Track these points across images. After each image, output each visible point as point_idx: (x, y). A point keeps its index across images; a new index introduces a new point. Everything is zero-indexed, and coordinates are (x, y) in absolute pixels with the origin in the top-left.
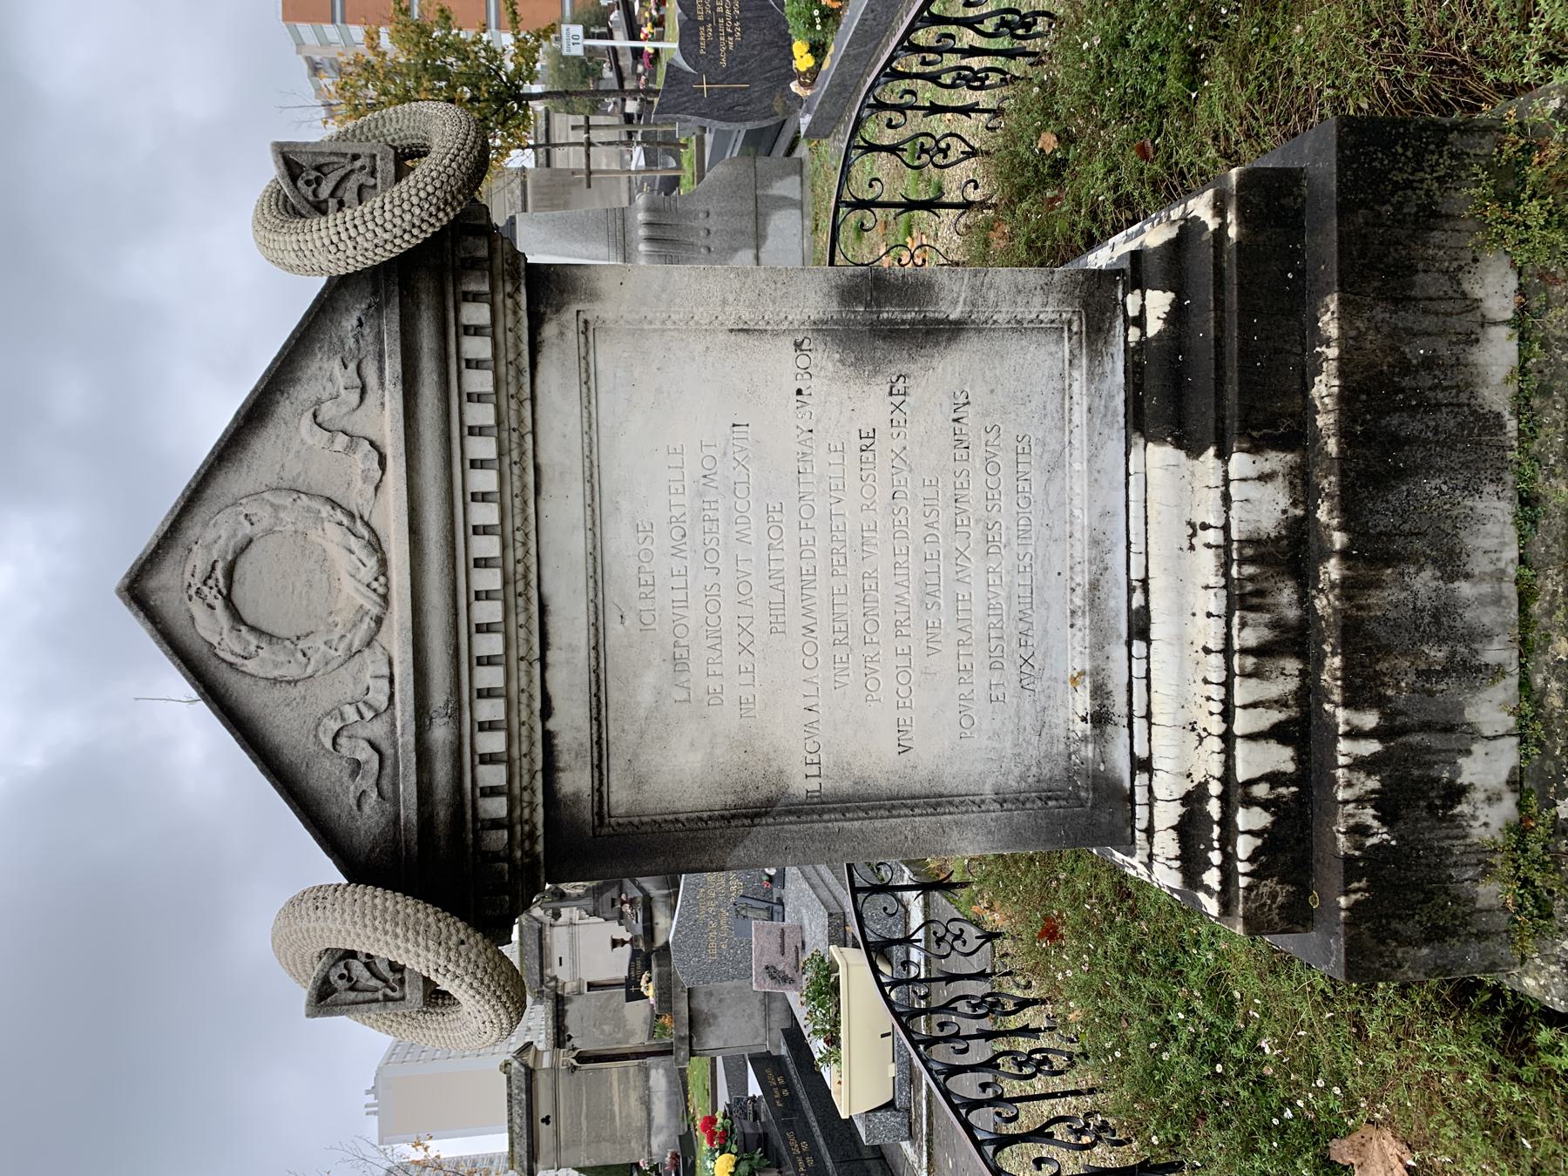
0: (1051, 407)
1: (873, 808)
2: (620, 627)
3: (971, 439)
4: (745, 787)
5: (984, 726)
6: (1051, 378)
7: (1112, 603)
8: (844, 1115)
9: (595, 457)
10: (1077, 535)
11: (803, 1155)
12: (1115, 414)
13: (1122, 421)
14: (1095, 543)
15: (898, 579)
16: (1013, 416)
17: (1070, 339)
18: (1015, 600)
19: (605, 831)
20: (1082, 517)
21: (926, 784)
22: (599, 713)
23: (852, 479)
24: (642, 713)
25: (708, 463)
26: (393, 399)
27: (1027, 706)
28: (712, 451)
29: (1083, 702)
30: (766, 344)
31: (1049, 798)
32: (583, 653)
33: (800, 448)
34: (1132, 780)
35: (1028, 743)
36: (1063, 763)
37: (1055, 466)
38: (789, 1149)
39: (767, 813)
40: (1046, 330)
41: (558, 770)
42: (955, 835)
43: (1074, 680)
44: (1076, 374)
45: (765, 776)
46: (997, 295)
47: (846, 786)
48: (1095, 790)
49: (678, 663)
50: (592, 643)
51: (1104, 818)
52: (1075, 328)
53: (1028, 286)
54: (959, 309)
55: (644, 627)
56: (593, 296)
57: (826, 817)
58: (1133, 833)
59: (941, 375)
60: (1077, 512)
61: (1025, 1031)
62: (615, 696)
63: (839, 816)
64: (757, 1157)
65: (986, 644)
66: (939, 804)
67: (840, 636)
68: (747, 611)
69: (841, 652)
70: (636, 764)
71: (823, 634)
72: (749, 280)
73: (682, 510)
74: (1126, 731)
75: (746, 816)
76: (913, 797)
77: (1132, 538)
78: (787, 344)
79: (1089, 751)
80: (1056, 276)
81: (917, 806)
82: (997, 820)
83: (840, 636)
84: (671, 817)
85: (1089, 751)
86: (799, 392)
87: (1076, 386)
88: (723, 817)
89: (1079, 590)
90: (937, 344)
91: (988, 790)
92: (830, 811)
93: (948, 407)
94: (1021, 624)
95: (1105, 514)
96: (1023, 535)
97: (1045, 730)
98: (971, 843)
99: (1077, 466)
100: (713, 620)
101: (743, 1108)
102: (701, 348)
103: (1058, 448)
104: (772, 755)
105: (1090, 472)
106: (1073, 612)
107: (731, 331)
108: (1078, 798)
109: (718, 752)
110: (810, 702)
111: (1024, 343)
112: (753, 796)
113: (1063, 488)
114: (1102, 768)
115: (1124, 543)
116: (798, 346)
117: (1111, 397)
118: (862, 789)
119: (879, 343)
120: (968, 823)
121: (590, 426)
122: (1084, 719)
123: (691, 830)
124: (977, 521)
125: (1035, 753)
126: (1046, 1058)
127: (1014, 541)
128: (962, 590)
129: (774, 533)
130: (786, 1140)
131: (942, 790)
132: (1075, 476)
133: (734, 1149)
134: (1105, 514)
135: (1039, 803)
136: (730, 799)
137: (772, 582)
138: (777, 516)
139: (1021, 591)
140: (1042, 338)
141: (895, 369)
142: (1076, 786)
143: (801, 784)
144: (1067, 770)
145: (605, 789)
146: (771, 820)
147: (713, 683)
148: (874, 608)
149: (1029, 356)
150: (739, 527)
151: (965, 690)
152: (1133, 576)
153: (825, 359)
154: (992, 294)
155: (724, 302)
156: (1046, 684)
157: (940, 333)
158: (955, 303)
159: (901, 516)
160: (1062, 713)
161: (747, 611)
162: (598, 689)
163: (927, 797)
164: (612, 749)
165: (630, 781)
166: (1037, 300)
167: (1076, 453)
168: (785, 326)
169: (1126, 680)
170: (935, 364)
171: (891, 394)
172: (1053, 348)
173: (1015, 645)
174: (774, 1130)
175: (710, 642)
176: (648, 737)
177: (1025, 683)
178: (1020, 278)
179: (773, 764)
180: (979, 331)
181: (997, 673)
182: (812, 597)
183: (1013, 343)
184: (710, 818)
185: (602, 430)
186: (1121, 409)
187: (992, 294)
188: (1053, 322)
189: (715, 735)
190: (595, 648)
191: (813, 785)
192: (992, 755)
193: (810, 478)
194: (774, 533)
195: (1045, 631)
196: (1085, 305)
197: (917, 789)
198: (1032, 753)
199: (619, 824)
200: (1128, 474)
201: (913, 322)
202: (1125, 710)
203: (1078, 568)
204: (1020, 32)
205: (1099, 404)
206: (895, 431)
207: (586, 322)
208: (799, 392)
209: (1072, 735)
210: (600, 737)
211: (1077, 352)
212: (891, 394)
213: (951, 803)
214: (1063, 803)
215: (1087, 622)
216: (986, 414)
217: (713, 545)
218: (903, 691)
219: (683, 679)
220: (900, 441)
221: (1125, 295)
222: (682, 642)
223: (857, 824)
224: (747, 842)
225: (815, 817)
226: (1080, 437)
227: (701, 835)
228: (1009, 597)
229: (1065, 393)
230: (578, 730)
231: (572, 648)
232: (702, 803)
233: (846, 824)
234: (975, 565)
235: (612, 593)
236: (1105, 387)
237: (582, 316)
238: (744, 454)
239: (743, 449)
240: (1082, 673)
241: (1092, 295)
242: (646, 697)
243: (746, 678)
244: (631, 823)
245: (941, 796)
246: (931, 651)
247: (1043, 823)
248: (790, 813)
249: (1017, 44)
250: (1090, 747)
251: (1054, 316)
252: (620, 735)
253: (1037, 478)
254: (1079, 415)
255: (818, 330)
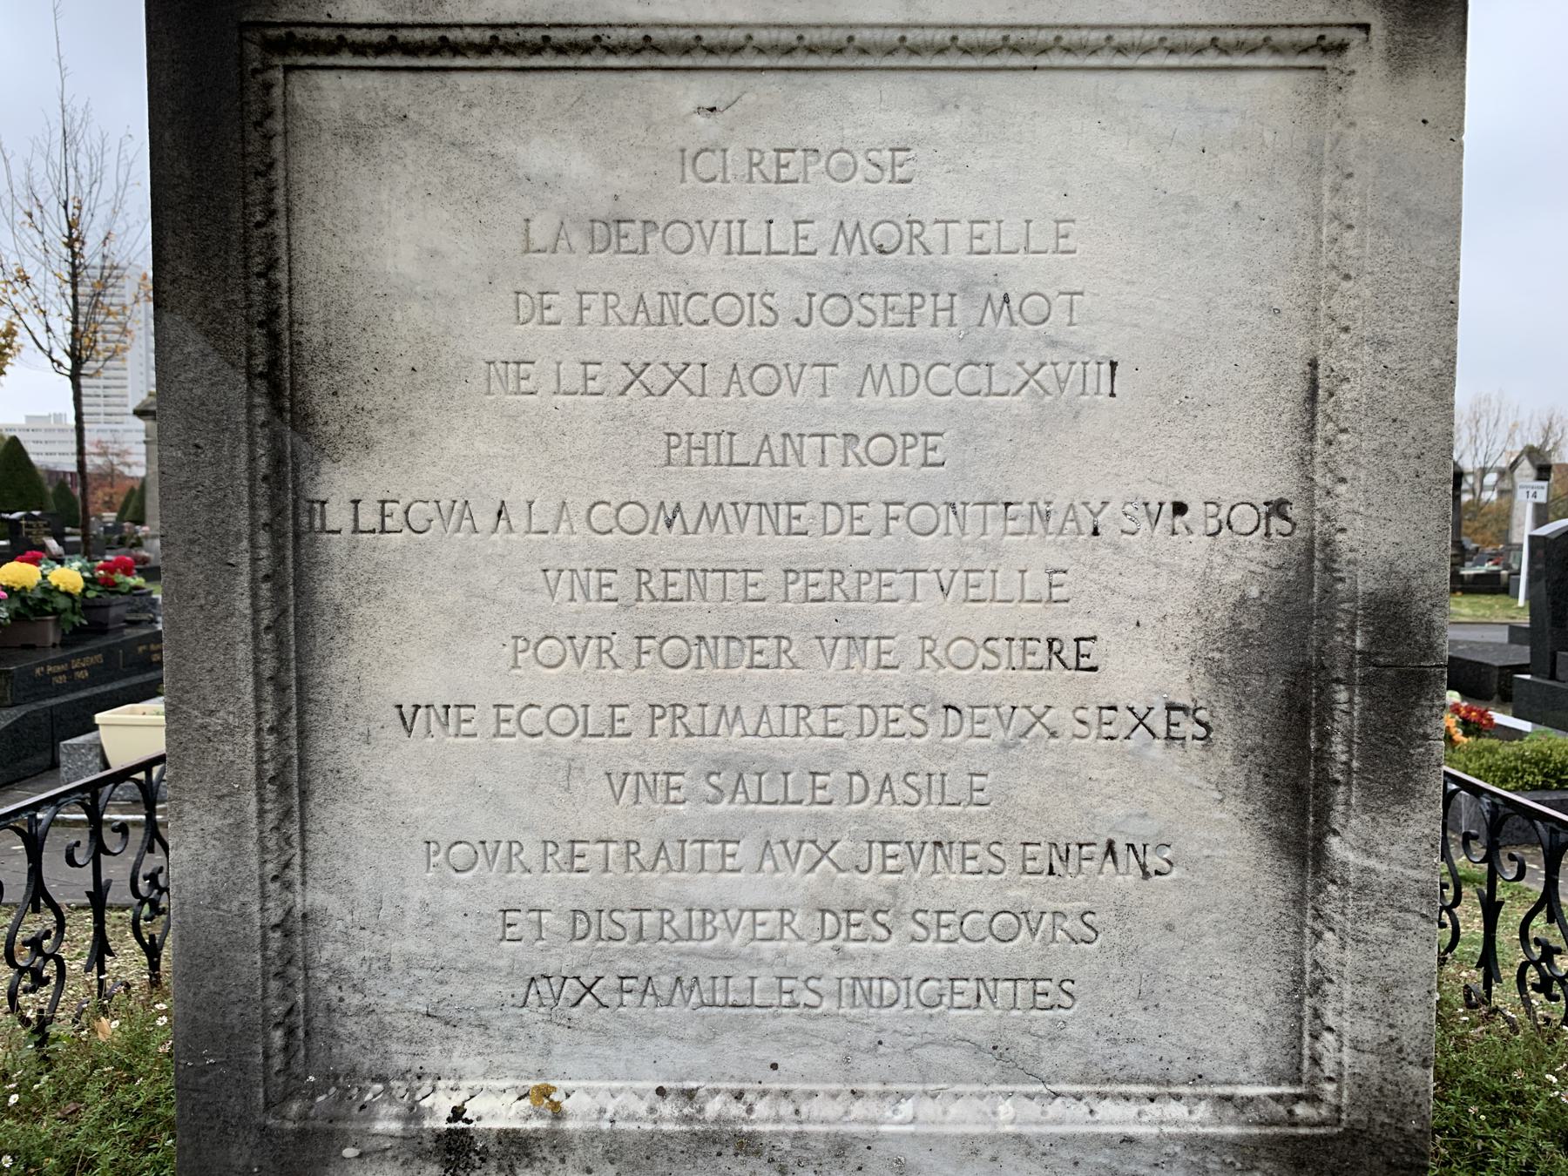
0: (1131, 1053)
1: (280, 643)
2: (689, 105)
3: (1070, 880)
4: (337, 367)
6: (1195, 1055)
8: (100, 718)
9: (1056, 59)
10: (858, 1109)
11: (70, 672)
15: (774, 714)
16: (1115, 971)
17: (1278, 1098)
19: (254, 52)
21: (330, 763)
23: (989, 619)
24: (505, 147)
25: (1033, 306)
27: (491, 989)
28: (1059, 316)
30: (1284, 440)
31: (290, 1033)
33: (1060, 504)
35: (412, 990)
36: (367, 1063)
37: (1005, 1061)
38: (81, 655)
39: (279, 411)
40: (1296, 1045)
42: (213, 822)
43: (545, 1092)
44: (1203, 1110)
45: (359, 410)
47: (332, 588)
48: (302, 1135)
49: (608, 229)
50: (658, 35)
52: (1301, 1110)
54: (1351, 857)
55: (688, 158)
56: (1401, 61)
57: (264, 538)
59: (1208, 821)
60: (907, 1108)
61: (101, 949)
63: (265, 566)
64: (76, 619)
65: (626, 900)
66: (284, 789)
67: (656, 585)
69: (622, 584)
70: (396, 132)
71: (664, 546)
72: (1425, 400)
75: (274, 363)
76: (302, 733)
78: (1281, 484)
79: (387, 1124)
80: (1416, 1072)
81: (282, 740)
82: (244, 916)
83: (656, 585)
84: (279, 200)
85: (387, 1124)
87: (1176, 1110)
88: (274, 314)
89: (737, 1109)
90: (1274, 810)
91: (315, 897)
92: (278, 549)
93: (1138, 831)
94: (667, 980)
96: (860, 990)
97: (438, 1027)
98: (195, 857)
99: (1006, 1109)
100: (699, 308)
101: (144, 609)
102: (1279, 300)
103: (1045, 1070)
104: (404, 428)
105: (993, 1139)
106: (690, 1095)
107: (1314, 365)
108: (288, 1097)
109: (415, 309)
110: (517, 518)
111: (1270, 997)
112: (318, 384)
113: (957, 1079)
114: (349, 1152)
116: (1278, 508)
118: (325, 621)
119: (1279, 684)
120: (239, 851)
122: (457, 1113)
123: (246, 240)
124: (893, 889)
125: (391, 1003)
126: (46, 981)
128: (745, 852)
129: (880, 447)
130: (92, 653)
131: (317, 798)
132: (985, 1106)
133: (91, 594)
135: (278, 1010)
136: (313, 334)
137: (776, 441)
138: (915, 454)
139: (739, 982)
142: (315, 1090)
143: (340, 489)
144: (352, 1072)
145: (346, 59)
146: (261, 415)
147: (564, 304)
148: (713, 658)
149: (1241, 1008)
151: (531, 854)
153: (1246, 564)
154: (1382, 930)
155: (1381, 344)
156: (537, 1031)
157: (1297, 817)
158: (1368, 849)
160: (474, 1063)
162: (560, 50)
163: (303, 764)
164: (432, 80)
165: (361, 116)
166: (1366, 1030)
170: (1231, 804)
171: (1171, 707)
172: (1257, 1061)
173: (625, 965)
174: (110, 640)
175: (652, 300)
176: (453, 158)
177: (543, 985)
178: (1415, 992)
179: (385, 431)
180: (1298, 901)
181: (564, 925)
182: (742, 524)
183: (1268, 975)
184: (273, 287)
187: (1382, 930)
188: (1316, 1061)
191: (338, 516)
192: (387, 911)
193: (994, 528)
194: (880, 447)
195: (654, 1033)
196: (1353, 1135)
197: (322, 744)
198: (390, 996)
199: (268, 87)
201: (1323, 757)
203: (786, 1109)
204: (1532, 975)
206: (1090, 715)
207: (1342, 47)
208: (1180, 508)
209: (427, 1084)
211: (1251, 1114)
212: (1171, 707)
213: (287, 814)
214: (277, 1063)
215: (668, 1127)
216: (1121, 913)
217: (860, 313)
218: (532, 719)
220: (1070, 726)
222: (654, 240)
223: (244, 605)
224: (214, 360)
225: (264, 515)
226: (1069, 1118)
227: (235, 258)
228: (725, 955)
229: (1162, 1086)
232: (306, 272)
233: (244, 581)
234: (799, 881)
237: (1356, 37)
238: (1051, 385)
239: (1061, 383)
240: (558, 1113)
241: (1375, 1149)
242: (539, 155)
243: (572, 379)
244: (269, 114)
245: (304, 795)
246: (616, 780)
247: (233, 1018)
248: (278, 461)
249: (1509, 974)
250: (395, 1127)
251: (1329, 1068)
252: (466, 99)
253: (982, 1022)
254: (1116, 1117)
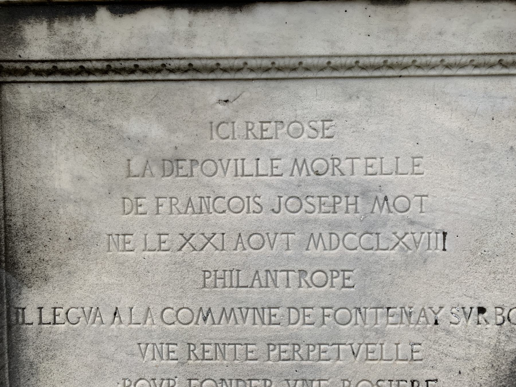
2: (214, 99)
9: (412, 72)
22: (117, 71)
24: (116, 122)
28: (415, 208)
32: (184, 51)
33: (416, 308)
41: (51, 22)
45: (42, 260)
49: (172, 164)
50: (196, 63)
55: (214, 127)
62: (138, 92)
70: (59, 115)
71: (202, 330)
73: (348, 172)
86: (482, 310)
104: (65, 270)
109: (71, 208)
118: (25, 371)
121: (447, 66)
147: (148, 203)
150: (326, 237)
161: (229, 244)
164: (78, 88)
165: (41, 107)
175: (196, 201)
176: (89, 128)
179: (56, 271)
182: (244, 319)
185: (441, 82)
189: (89, 204)
190: (190, 68)
191: (31, 316)
208: (482, 310)
210: (89, 72)
217: (306, 206)
219: (155, 169)
222: (196, 170)
230: (96, 45)
231: (190, 37)
235: (254, 90)
238: (411, 245)
239: (417, 243)
242: (134, 126)
252: (94, 97)
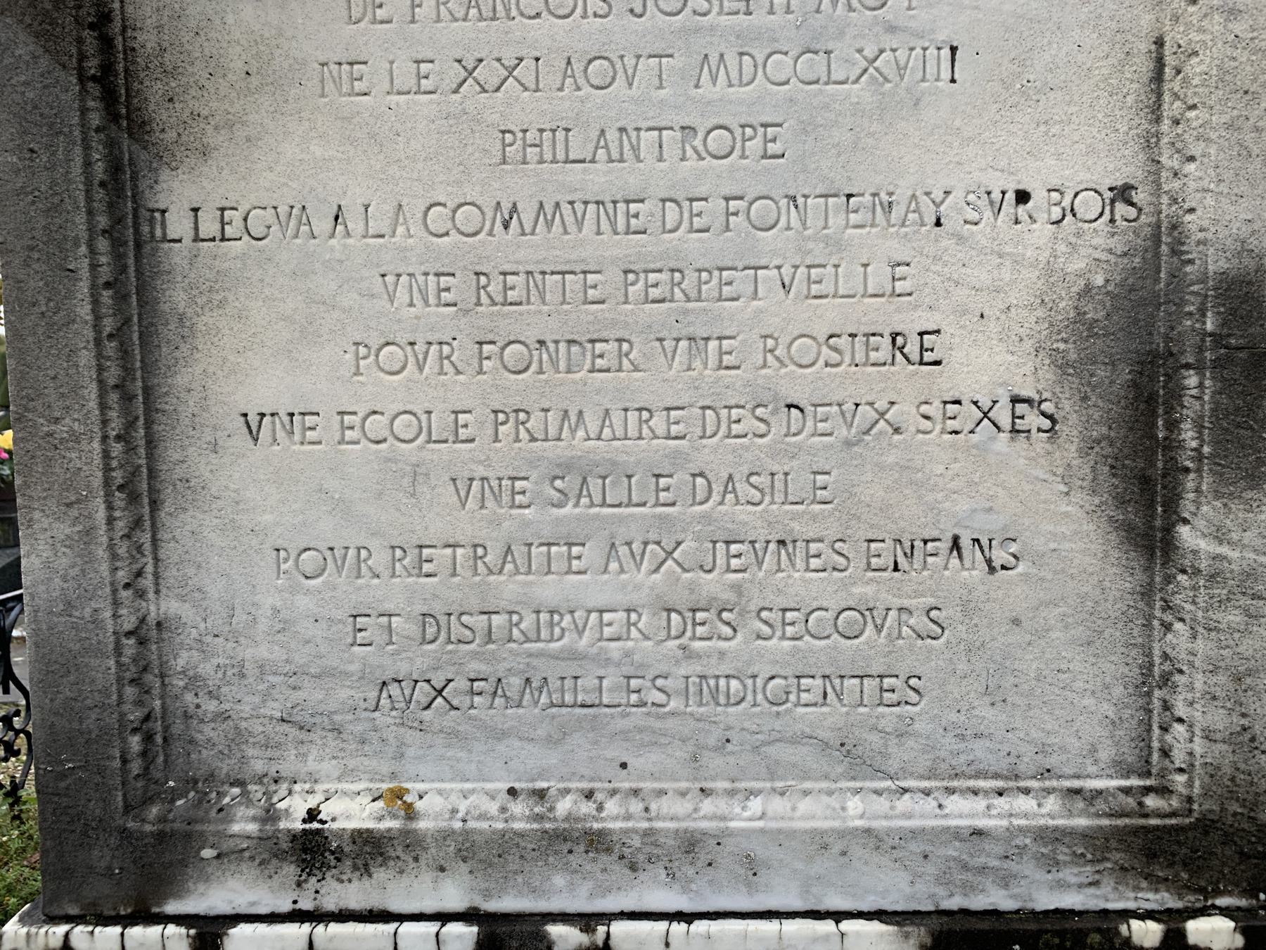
0: (979, 750)
3: (914, 576)
4: (172, 73)
5: (303, 602)
6: (1042, 750)
7: (559, 880)
10: (707, 806)
12: (968, 889)
13: (953, 903)
14: (691, 844)
15: (617, 417)
16: (962, 667)
17: (1127, 791)
18: (571, 669)
20: (745, 816)
21: (179, 472)
23: (830, 315)
26: (732, 691)
27: (343, 694)
29: (351, 811)
31: (148, 738)
34: (179, 920)
35: (266, 696)
36: (224, 767)
37: (853, 759)
39: (114, 117)
42: (63, 529)
43: (398, 794)
44: (1052, 804)
46: (1232, 630)
47: (176, 297)
48: (161, 837)
51: (101, 856)
52: (1151, 802)
53: (1249, 699)
54: (1202, 544)
57: (103, 244)
58: (68, 919)
59: (1052, 510)
60: (756, 805)
63: (105, 273)
65: (474, 603)
66: (134, 498)
67: (495, 288)
68: (550, 79)
69: (461, 287)
71: (502, 249)
74: (285, 906)
76: (151, 443)
77: (700, 926)
78: (1126, 168)
79: (244, 825)
81: (130, 449)
82: (96, 621)
83: (495, 288)
85: (244, 825)
87: (1025, 804)
89: (587, 808)
90: (1121, 502)
91: (170, 606)
92: (118, 257)
93: (984, 525)
94: (516, 682)
95: (752, 867)
96: (706, 688)
97: (293, 732)
98: (47, 565)
99: (855, 805)
103: (893, 765)
104: (240, 133)
105: (842, 834)
106: (541, 794)
107: (1160, 43)
108: (148, 801)
111: (1118, 691)
112: (154, 90)
113: (806, 777)
114: (207, 853)
115: (686, 905)
116: (1123, 193)
117: (1005, 881)
118: (169, 331)
119: (1125, 374)
120: (89, 559)
122: (312, 815)
124: (737, 588)
125: (246, 709)
127: (696, 668)
131: (168, 507)
132: (833, 801)
134: (752, 867)
135: (135, 715)
136: (147, 40)
137: (612, 135)
138: (754, 146)
139: (589, 682)
140: (1130, 726)
141: (1068, 408)
142: (174, 795)
143: (179, 196)
146: (95, 119)
148: (554, 363)
149: (1089, 701)
151: (379, 559)
152: (618, 928)
153: (1091, 252)
154: (1233, 617)
156: (390, 735)
158: (1219, 536)
159: (749, 424)
160: (329, 767)
161: (550, 79)
163: (152, 474)
166: (1219, 719)
167: (882, 804)
168: (1169, 160)
169: (396, 906)
170: (1078, 497)
171: (1015, 400)
172: (1105, 754)
173: (475, 667)
177: (394, 689)
180: (1147, 594)
181: (413, 629)
182: (580, 224)
183: (1116, 669)
186: (978, 903)
187: (1233, 617)
188: (1165, 753)
191: (178, 225)
192: (240, 618)
193: (836, 221)
195: (503, 735)
196: (1206, 825)
198: (249, 704)
200: (838, 916)
201: (1171, 445)
202: (330, 905)
203: (636, 806)
205: (989, 855)
206: (934, 410)
209: (283, 788)
211: (1101, 805)
213: (137, 523)
214: (136, 767)
215: (518, 826)
216: (968, 608)
218: (376, 425)
221: (1226, 912)
223: (84, 311)
224: (44, 62)
225: (103, 221)
226: (917, 812)
228: (573, 655)
229: (1010, 780)
233: (84, 287)
234: (645, 581)
236: (1028, 868)
238: (891, 73)
239: (901, 69)
240: (410, 813)
241: (1227, 839)
243: (405, 74)
245: (155, 504)
246: (462, 485)
248: (115, 168)
250: (252, 828)
251: (1179, 758)
254: (964, 811)
255: (1156, 239)
